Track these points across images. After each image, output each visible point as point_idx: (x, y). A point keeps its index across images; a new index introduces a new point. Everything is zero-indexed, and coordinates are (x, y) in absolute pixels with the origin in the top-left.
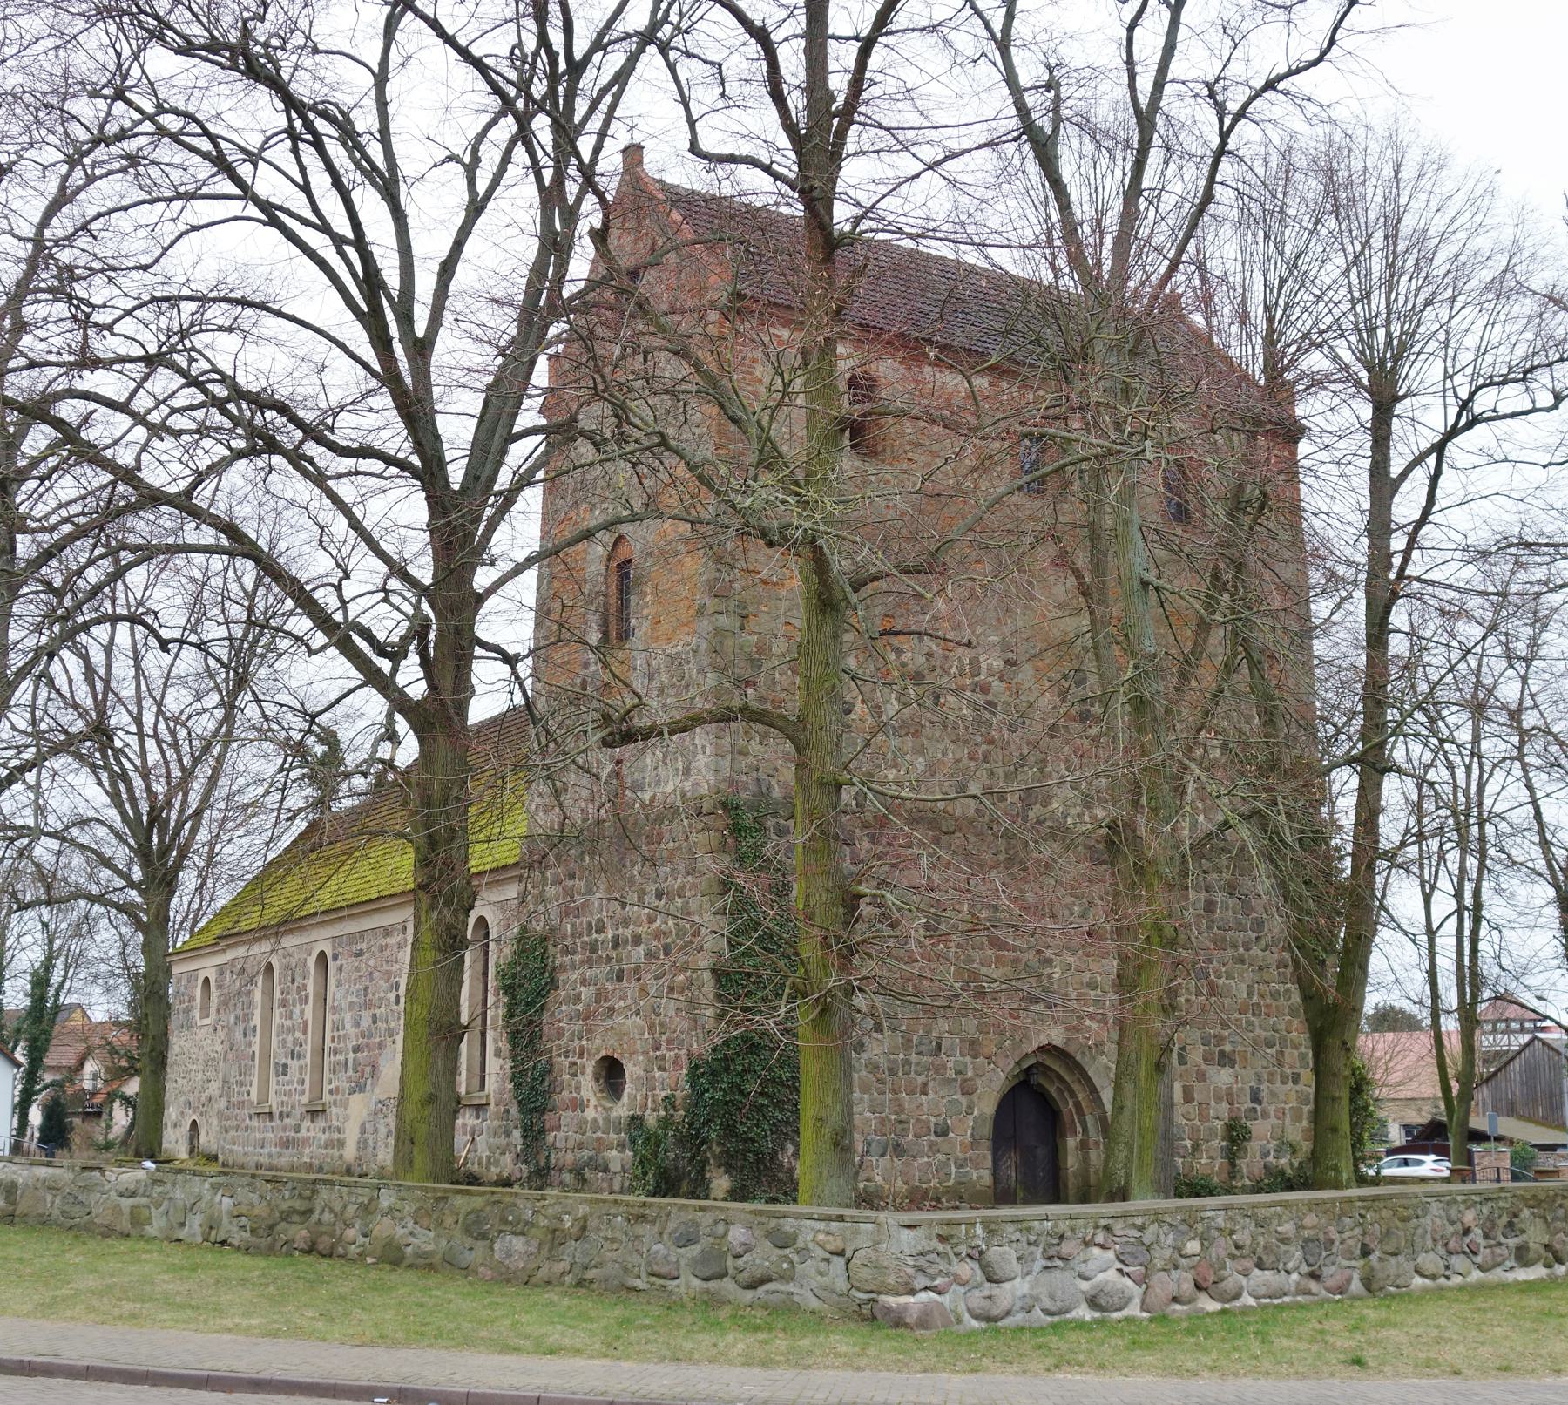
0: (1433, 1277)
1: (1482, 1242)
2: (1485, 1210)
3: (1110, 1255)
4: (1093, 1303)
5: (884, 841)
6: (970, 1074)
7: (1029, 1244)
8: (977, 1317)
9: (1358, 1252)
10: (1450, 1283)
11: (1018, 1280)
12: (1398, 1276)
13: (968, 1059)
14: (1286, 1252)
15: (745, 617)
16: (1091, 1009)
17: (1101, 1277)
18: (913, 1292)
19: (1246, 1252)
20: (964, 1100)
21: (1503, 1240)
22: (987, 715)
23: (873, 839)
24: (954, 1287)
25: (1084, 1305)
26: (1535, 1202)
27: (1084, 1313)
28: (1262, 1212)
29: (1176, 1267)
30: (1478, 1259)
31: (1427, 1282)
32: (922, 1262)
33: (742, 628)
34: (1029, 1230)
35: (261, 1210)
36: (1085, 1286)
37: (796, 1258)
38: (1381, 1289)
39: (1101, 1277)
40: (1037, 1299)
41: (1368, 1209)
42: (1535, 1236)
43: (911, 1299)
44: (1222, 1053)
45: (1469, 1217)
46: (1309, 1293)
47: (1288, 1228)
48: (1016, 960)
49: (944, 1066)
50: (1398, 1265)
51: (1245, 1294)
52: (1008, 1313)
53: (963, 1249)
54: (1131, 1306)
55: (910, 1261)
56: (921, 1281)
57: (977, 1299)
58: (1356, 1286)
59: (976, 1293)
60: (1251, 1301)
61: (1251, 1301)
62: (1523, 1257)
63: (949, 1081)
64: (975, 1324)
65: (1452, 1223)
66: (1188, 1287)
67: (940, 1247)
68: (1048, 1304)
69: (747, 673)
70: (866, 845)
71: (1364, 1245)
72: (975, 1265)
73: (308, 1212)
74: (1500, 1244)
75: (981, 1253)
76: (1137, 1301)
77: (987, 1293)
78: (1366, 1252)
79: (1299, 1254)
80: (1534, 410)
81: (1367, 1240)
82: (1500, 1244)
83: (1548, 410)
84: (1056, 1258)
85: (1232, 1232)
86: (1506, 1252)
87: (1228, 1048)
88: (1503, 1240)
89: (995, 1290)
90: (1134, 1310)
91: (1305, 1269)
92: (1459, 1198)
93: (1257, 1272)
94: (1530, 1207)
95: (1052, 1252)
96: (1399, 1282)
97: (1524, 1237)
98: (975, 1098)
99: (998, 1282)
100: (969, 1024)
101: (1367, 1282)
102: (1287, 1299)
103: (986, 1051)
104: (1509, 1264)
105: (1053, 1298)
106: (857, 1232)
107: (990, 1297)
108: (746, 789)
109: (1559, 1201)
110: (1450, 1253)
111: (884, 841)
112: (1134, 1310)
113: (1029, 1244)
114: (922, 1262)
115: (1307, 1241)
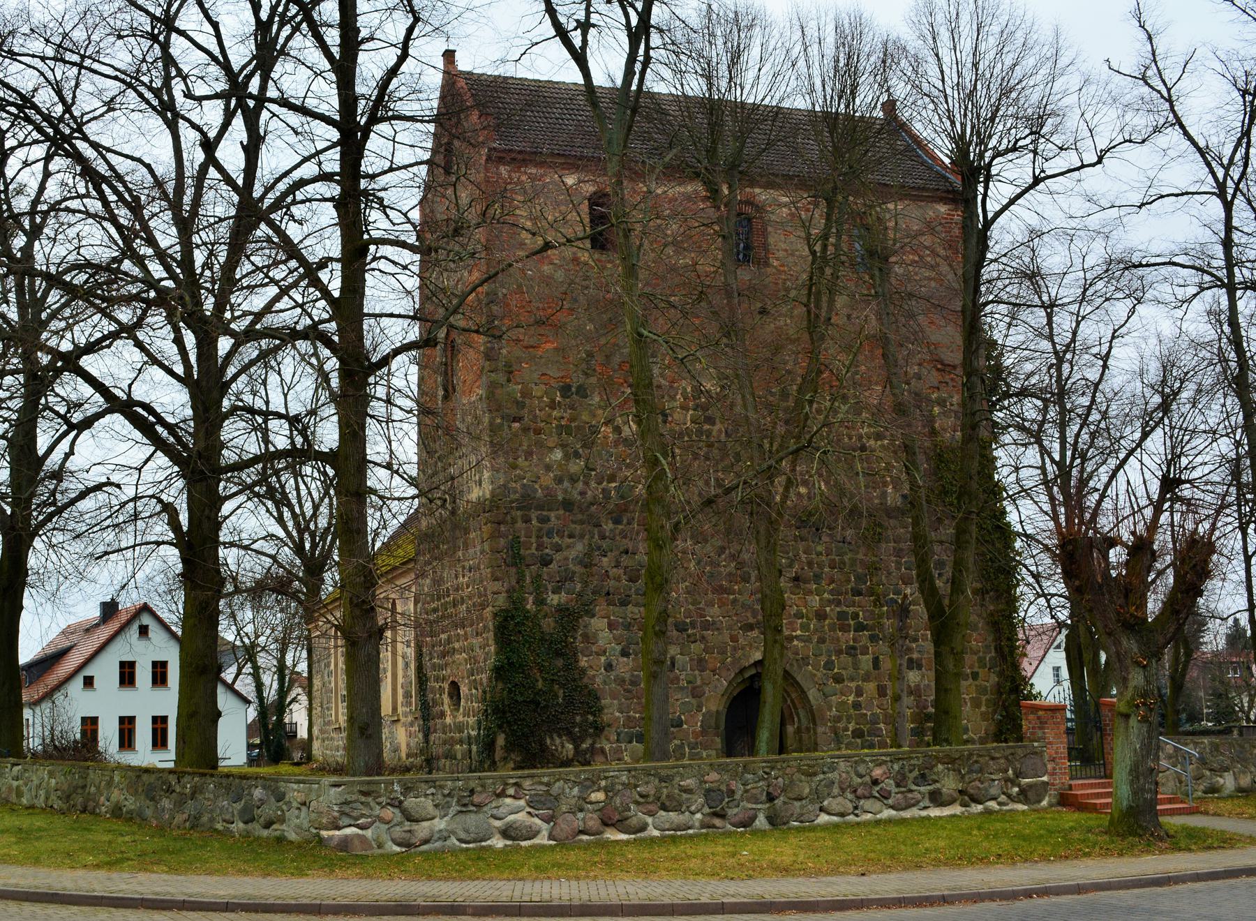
0: (842, 815)
1: (894, 790)
2: (896, 767)
3: (522, 802)
4: (505, 833)
5: (625, 521)
6: (699, 682)
7: (444, 796)
8: (399, 845)
9: (764, 798)
10: (858, 819)
11: (437, 820)
12: (802, 815)
13: (697, 672)
14: (688, 799)
15: (511, 372)
16: (799, 632)
17: (511, 818)
18: (339, 828)
19: (651, 799)
20: (694, 701)
21: (914, 787)
22: (707, 427)
23: (617, 521)
24: (377, 824)
25: (498, 836)
26: (950, 760)
27: (498, 843)
28: (663, 773)
29: (581, 810)
30: (890, 802)
31: (835, 819)
32: (346, 809)
33: (509, 381)
34: (442, 787)
35: (65, 787)
36: (498, 823)
37: (285, 807)
38: (784, 824)
39: (511, 818)
40: (454, 833)
41: (772, 768)
42: (949, 784)
43: (337, 833)
44: (910, 661)
45: (877, 772)
46: (714, 826)
47: (690, 782)
48: (735, 601)
49: (678, 679)
50: (802, 807)
51: (651, 827)
52: (426, 842)
53: (383, 800)
54: (539, 836)
55: (336, 808)
56: (346, 821)
57: (398, 832)
58: (761, 822)
59: (398, 828)
60: (656, 833)
61: (656, 833)
62: (937, 799)
63: (682, 688)
64: (398, 849)
65: (861, 776)
66: (594, 823)
67: (363, 799)
68: (463, 835)
69: (513, 411)
70: (611, 526)
71: (768, 794)
72: (397, 811)
73: (84, 787)
74: (911, 791)
75: (401, 802)
76: (545, 833)
77: (407, 828)
78: (771, 798)
79: (701, 800)
80: (1083, 166)
81: (771, 789)
82: (911, 791)
83: (1093, 165)
84: (468, 803)
85: (636, 786)
86: (919, 796)
87: (915, 656)
88: (914, 787)
89: (415, 827)
90: (542, 840)
91: (707, 810)
92: (867, 759)
93: (662, 813)
94: (943, 763)
95: (466, 801)
96: (805, 817)
97: (938, 785)
98: (703, 699)
99: (417, 821)
100: (696, 648)
101: (771, 820)
102: (691, 831)
103: (711, 666)
104: (922, 804)
105: (467, 831)
106: (310, 790)
107: (410, 831)
108: (516, 492)
109: (975, 758)
110: (858, 798)
111: (625, 521)
112: (542, 840)
113: (444, 796)
114: (346, 809)
115: (708, 791)
